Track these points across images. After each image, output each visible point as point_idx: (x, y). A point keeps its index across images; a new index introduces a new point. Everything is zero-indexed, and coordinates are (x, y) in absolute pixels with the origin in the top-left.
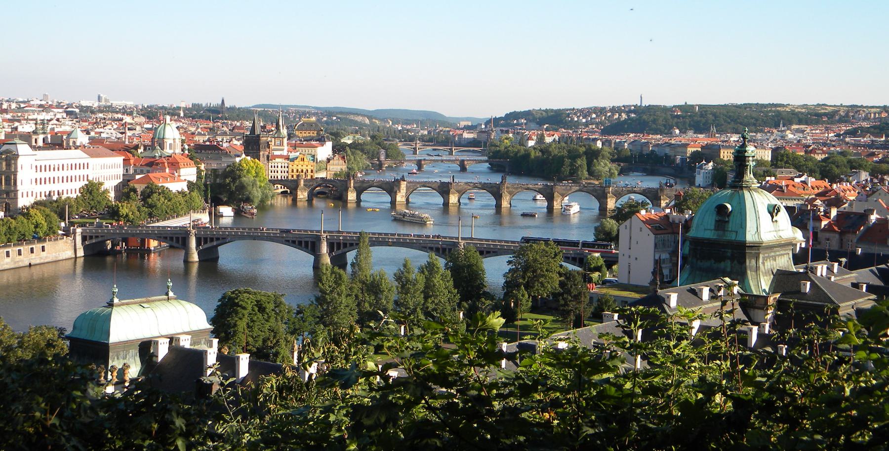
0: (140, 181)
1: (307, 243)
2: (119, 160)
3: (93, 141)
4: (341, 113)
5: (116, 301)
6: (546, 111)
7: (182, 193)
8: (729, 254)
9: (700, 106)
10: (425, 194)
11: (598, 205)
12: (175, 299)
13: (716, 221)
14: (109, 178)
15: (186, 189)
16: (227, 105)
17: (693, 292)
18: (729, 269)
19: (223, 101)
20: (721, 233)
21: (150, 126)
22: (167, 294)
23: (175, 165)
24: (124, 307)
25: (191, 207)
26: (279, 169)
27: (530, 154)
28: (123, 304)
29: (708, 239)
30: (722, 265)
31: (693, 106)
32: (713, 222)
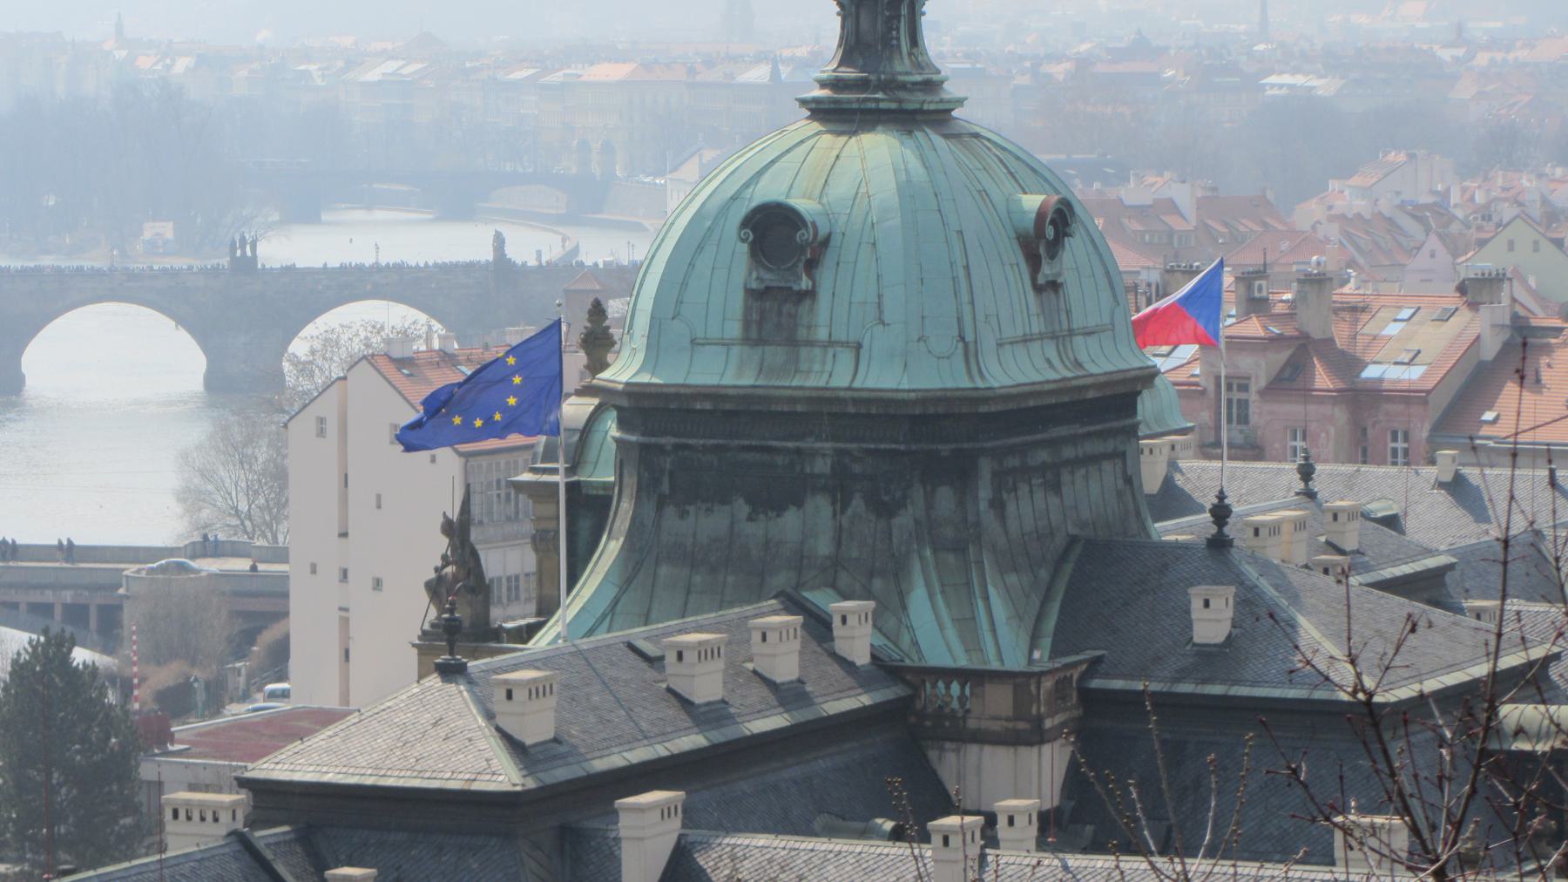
8: (822, 466)
13: (750, 293)
18: (823, 546)
29: (713, 395)
32: (737, 301)
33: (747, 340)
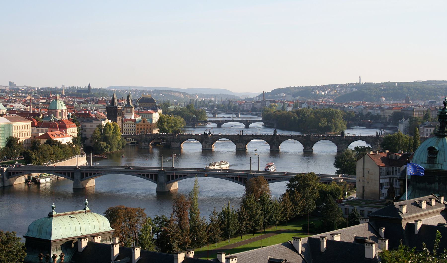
0: (42, 137)
1: (69, 173)
2: (29, 123)
3: (9, 111)
4: (165, 91)
5: (54, 213)
6: (298, 88)
7: (69, 144)
8: (437, 179)
9: (398, 83)
10: (224, 144)
11: (336, 148)
12: (90, 212)
13: (428, 157)
14: (23, 135)
15: (71, 142)
16: (92, 87)
17: (415, 204)
19: (89, 84)
20: (431, 165)
21: (45, 101)
22: (85, 209)
23: (63, 126)
24: (59, 217)
25: (74, 153)
26: (130, 128)
27: (298, 118)
28: (59, 215)
30: (433, 185)
31: (394, 83)
32: (426, 159)
33: (428, 163)
